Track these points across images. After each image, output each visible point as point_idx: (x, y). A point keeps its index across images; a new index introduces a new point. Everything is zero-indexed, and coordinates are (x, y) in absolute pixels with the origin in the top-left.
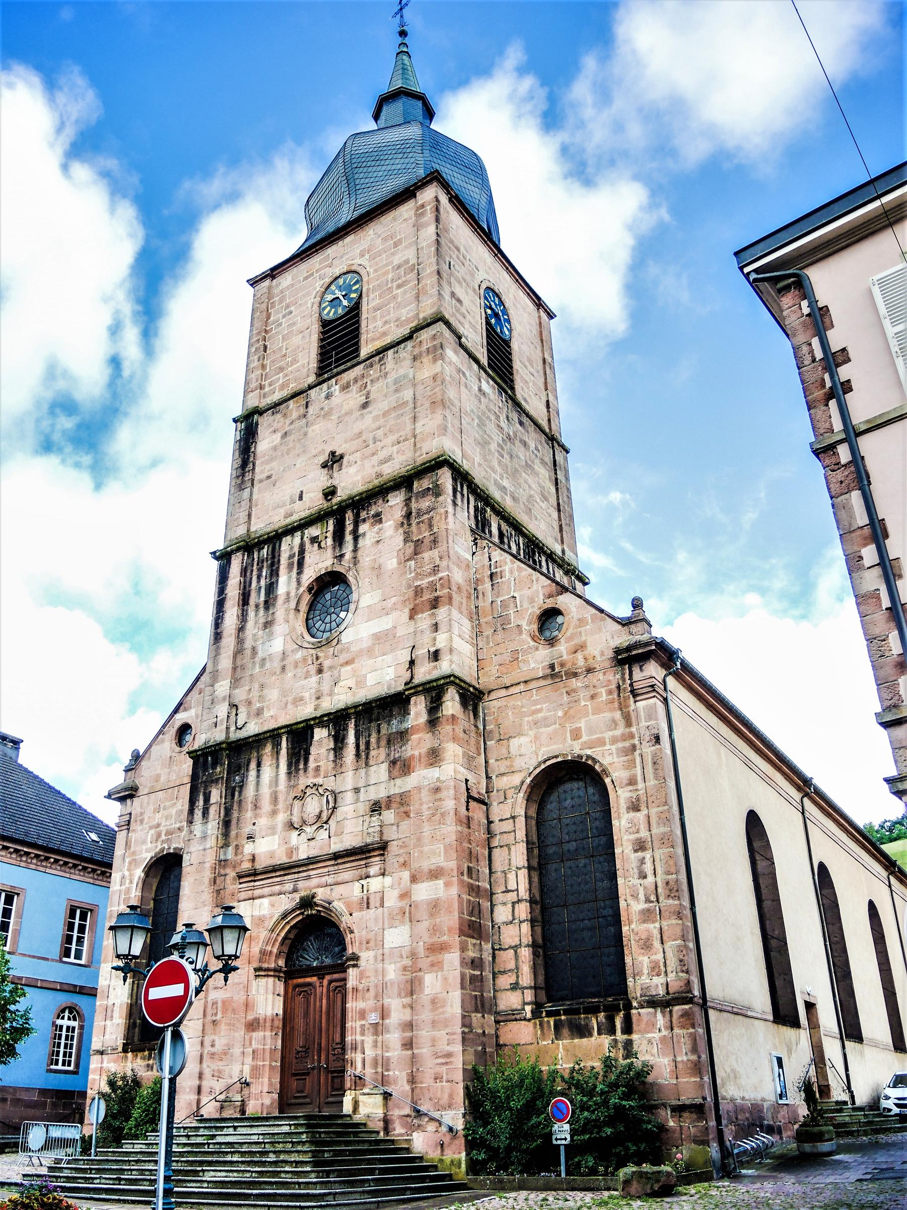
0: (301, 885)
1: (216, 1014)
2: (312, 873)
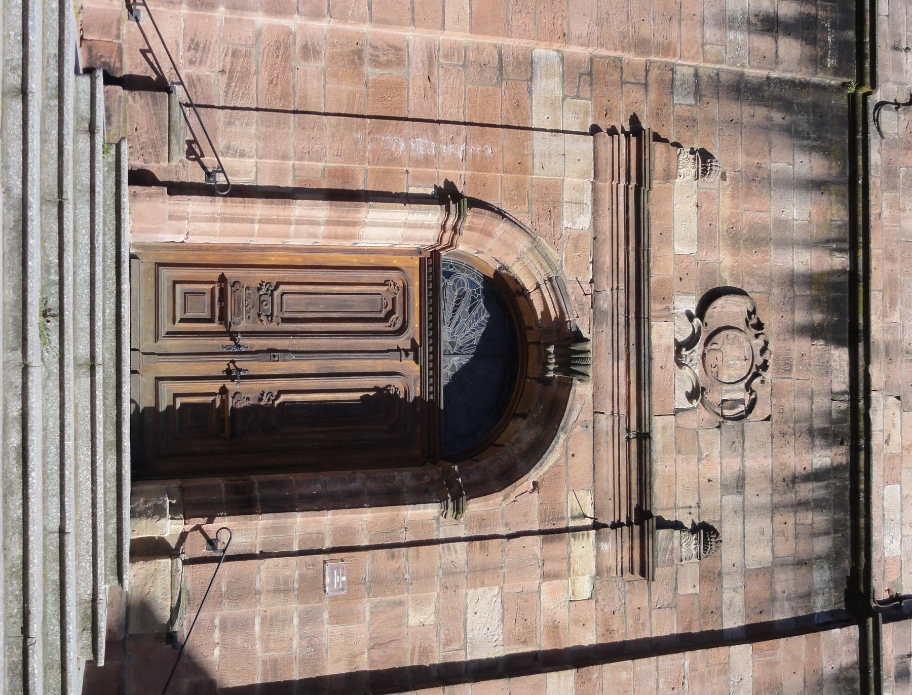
0: (606, 331)
1: (375, 62)
2: (622, 364)
